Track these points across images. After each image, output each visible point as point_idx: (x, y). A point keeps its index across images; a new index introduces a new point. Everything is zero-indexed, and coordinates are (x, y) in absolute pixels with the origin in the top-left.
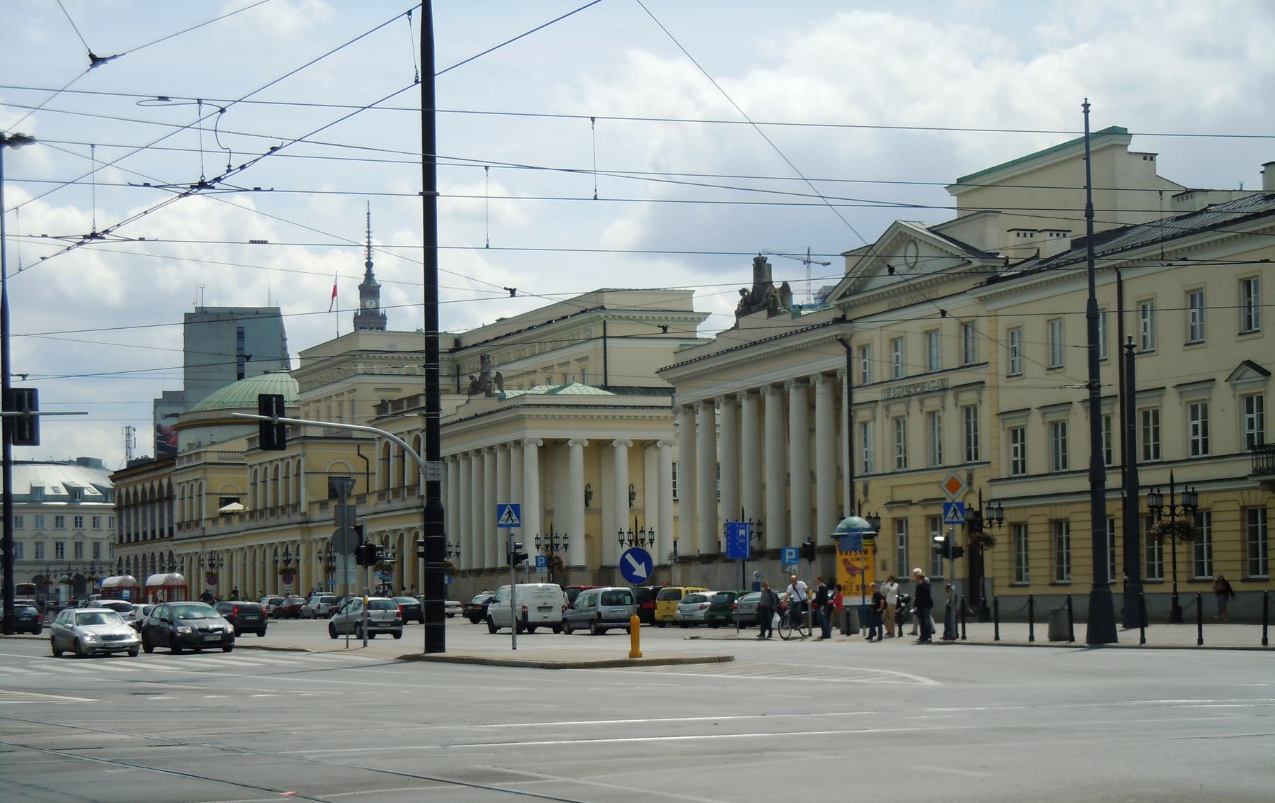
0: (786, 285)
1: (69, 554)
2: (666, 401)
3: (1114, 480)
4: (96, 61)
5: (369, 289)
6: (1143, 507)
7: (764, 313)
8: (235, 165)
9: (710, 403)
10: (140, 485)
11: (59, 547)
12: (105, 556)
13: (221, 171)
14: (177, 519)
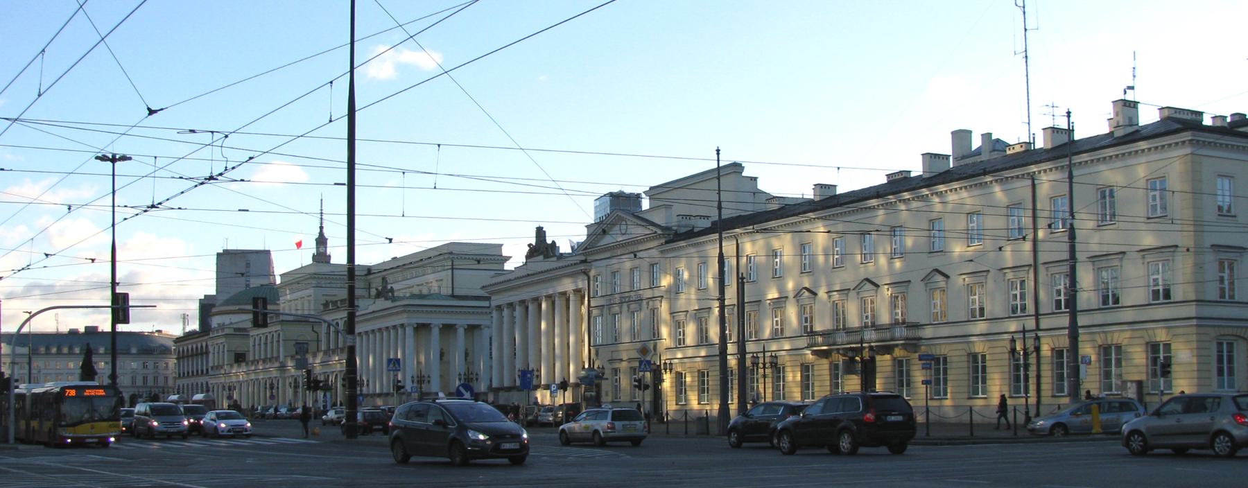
0: (554, 242)
1: (150, 383)
2: (486, 304)
3: (731, 348)
4: (151, 112)
5: (321, 241)
6: (748, 363)
7: (541, 257)
8: (229, 167)
9: (511, 305)
10: (190, 345)
11: (145, 378)
12: (171, 383)
13: (222, 170)
14: (211, 364)
